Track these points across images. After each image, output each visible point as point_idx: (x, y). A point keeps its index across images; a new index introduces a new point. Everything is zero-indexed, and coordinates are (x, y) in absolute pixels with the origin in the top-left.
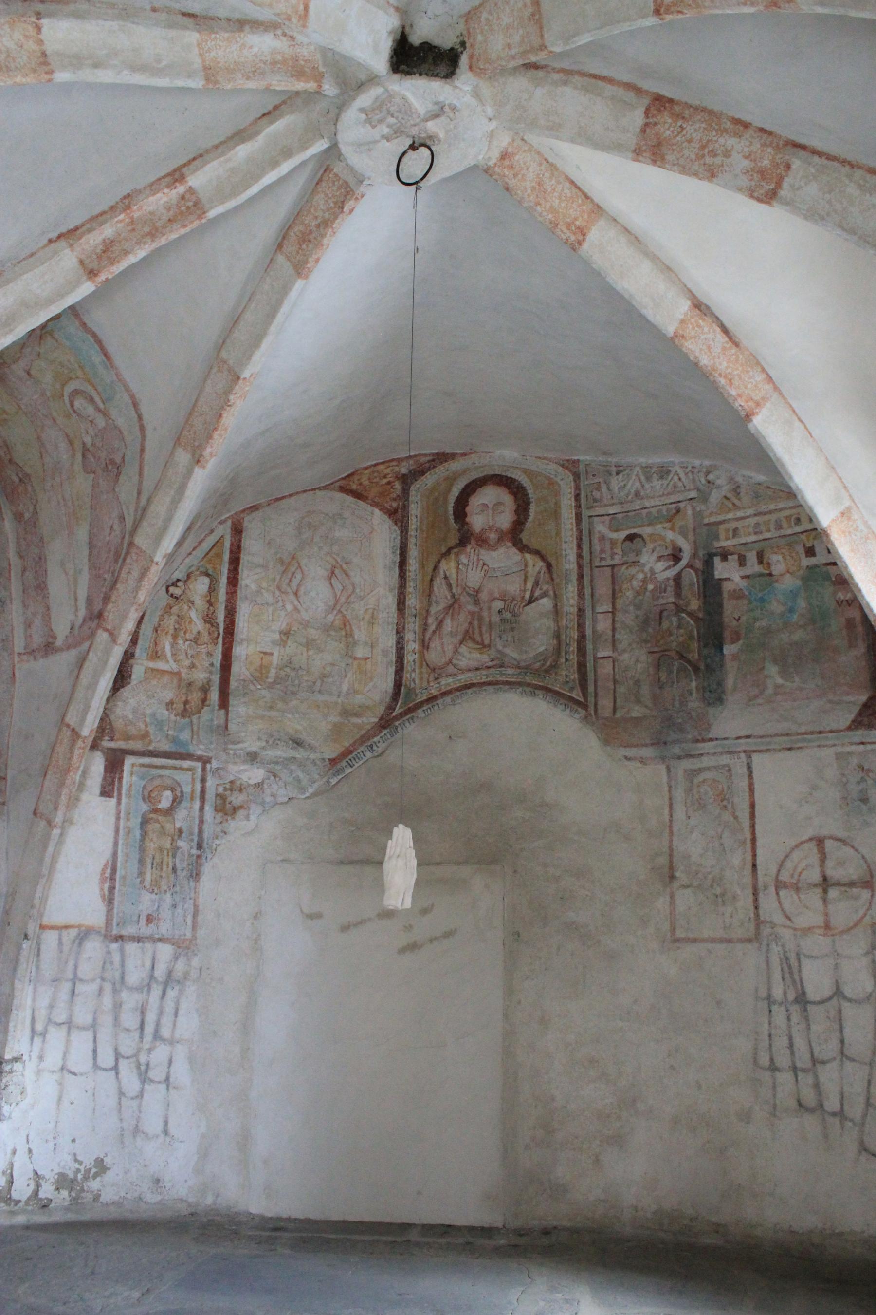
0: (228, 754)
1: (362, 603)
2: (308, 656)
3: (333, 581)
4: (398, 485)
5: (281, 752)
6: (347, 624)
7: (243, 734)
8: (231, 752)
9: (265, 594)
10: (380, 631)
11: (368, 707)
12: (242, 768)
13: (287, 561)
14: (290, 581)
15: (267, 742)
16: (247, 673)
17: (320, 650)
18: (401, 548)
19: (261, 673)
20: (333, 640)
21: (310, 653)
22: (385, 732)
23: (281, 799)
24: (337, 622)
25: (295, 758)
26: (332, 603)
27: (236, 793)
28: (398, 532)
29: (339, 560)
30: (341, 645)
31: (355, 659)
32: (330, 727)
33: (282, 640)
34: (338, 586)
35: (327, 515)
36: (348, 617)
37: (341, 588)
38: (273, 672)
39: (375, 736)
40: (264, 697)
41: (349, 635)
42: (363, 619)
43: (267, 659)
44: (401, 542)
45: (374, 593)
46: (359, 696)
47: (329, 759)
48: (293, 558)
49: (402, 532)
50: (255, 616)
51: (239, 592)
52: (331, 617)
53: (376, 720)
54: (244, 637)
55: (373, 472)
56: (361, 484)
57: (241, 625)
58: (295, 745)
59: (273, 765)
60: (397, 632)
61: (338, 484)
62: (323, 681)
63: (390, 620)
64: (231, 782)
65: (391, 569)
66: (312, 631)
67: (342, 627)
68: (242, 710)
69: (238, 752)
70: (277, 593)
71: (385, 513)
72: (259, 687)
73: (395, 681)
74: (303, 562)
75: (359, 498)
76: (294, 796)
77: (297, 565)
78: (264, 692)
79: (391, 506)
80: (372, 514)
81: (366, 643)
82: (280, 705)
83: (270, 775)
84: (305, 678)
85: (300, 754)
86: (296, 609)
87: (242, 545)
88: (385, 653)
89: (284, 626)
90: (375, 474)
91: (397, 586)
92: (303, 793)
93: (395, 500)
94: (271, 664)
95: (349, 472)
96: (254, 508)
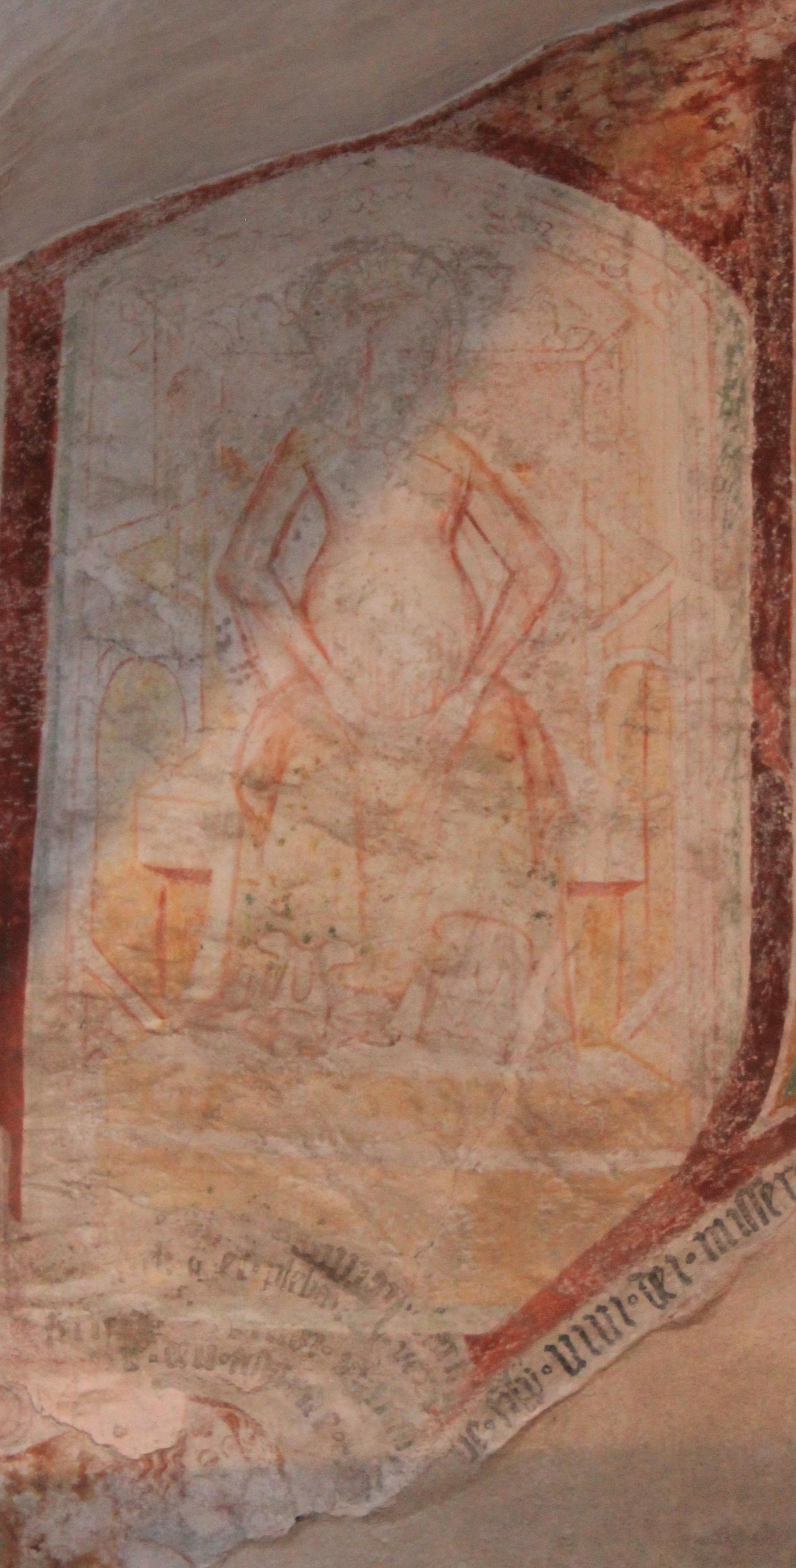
0: (25, 1323)
1: (594, 639)
2: (364, 878)
3: (464, 550)
4: (738, 114)
5: (257, 1313)
6: (534, 736)
7: (88, 1235)
8: (38, 1316)
9: (167, 613)
10: (679, 762)
11: (638, 1104)
12: (86, 1384)
13: (256, 467)
14: (275, 553)
15: (195, 1267)
16: (99, 964)
17: (412, 852)
18: (762, 393)
19: (161, 963)
20: (470, 806)
21: (375, 866)
22: (717, 1210)
23: (259, 1525)
24: (487, 732)
25: (320, 1337)
26: (465, 641)
27: (62, 1502)
28: (748, 322)
29: (487, 453)
30: (511, 832)
31: (573, 888)
32: (470, 1194)
33: (247, 812)
34: (487, 571)
35: (425, 254)
36: (534, 703)
37: (499, 575)
38: (211, 960)
39: (672, 1230)
40: (177, 1068)
41: (544, 783)
42: (603, 707)
43: (183, 896)
44: (763, 364)
45: (647, 594)
46: (594, 1057)
47: (472, 1340)
48: (285, 450)
49: (763, 319)
50: (126, 710)
51: (51, 606)
52: (458, 710)
53: (678, 1159)
54: (80, 803)
55: (628, 57)
56: (572, 113)
57: (66, 752)
58: (318, 1278)
59: (221, 1370)
60: (758, 767)
61: (470, 116)
62: (430, 989)
63: (724, 713)
64: (42, 1450)
65: (718, 487)
66: (381, 770)
67: (509, 747)
68: (83, 1128)
69: (65, 1314)
70: (221, 608)
71: (686, 239)
72: (154, 1023)
73: (756, 985)
74: (329, 468)
75: (566, 178)
76: (321, 1507)
77: (300, 480)
78: (174, 1047)
79: (711, 206)
80: (628, 242)
81: (618, 820)
82: (249, 1102)
83: (207, 1410)
84: (353, 980)
85: (339, 1318)
86: (304, 674)
87: (61, 400)
88: (704, 859)
89: (253, 754)
90: (636, 68)
91: (749, 560)
92: (365, 1493)
93: (726, 177)
94: (201, 917)
95: (520, 63)
96: (104, 237)
